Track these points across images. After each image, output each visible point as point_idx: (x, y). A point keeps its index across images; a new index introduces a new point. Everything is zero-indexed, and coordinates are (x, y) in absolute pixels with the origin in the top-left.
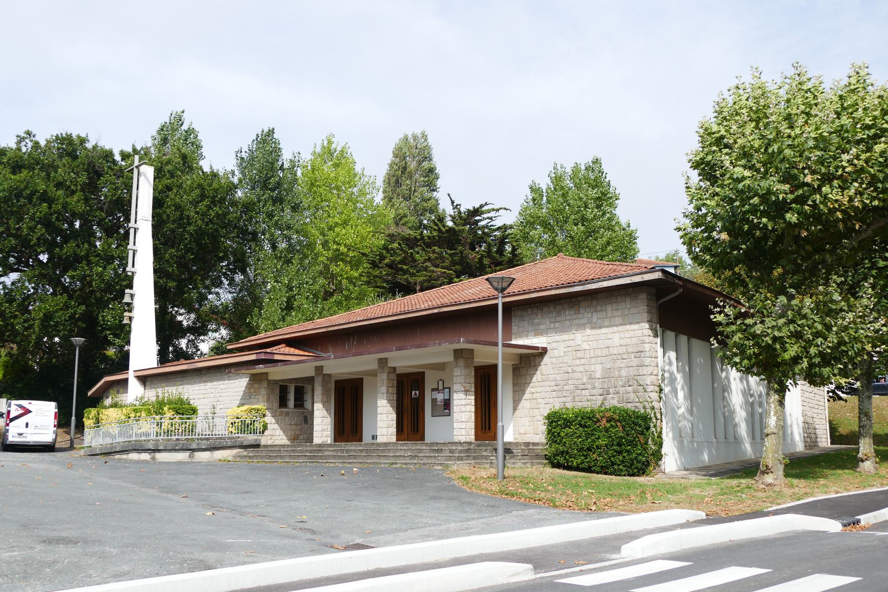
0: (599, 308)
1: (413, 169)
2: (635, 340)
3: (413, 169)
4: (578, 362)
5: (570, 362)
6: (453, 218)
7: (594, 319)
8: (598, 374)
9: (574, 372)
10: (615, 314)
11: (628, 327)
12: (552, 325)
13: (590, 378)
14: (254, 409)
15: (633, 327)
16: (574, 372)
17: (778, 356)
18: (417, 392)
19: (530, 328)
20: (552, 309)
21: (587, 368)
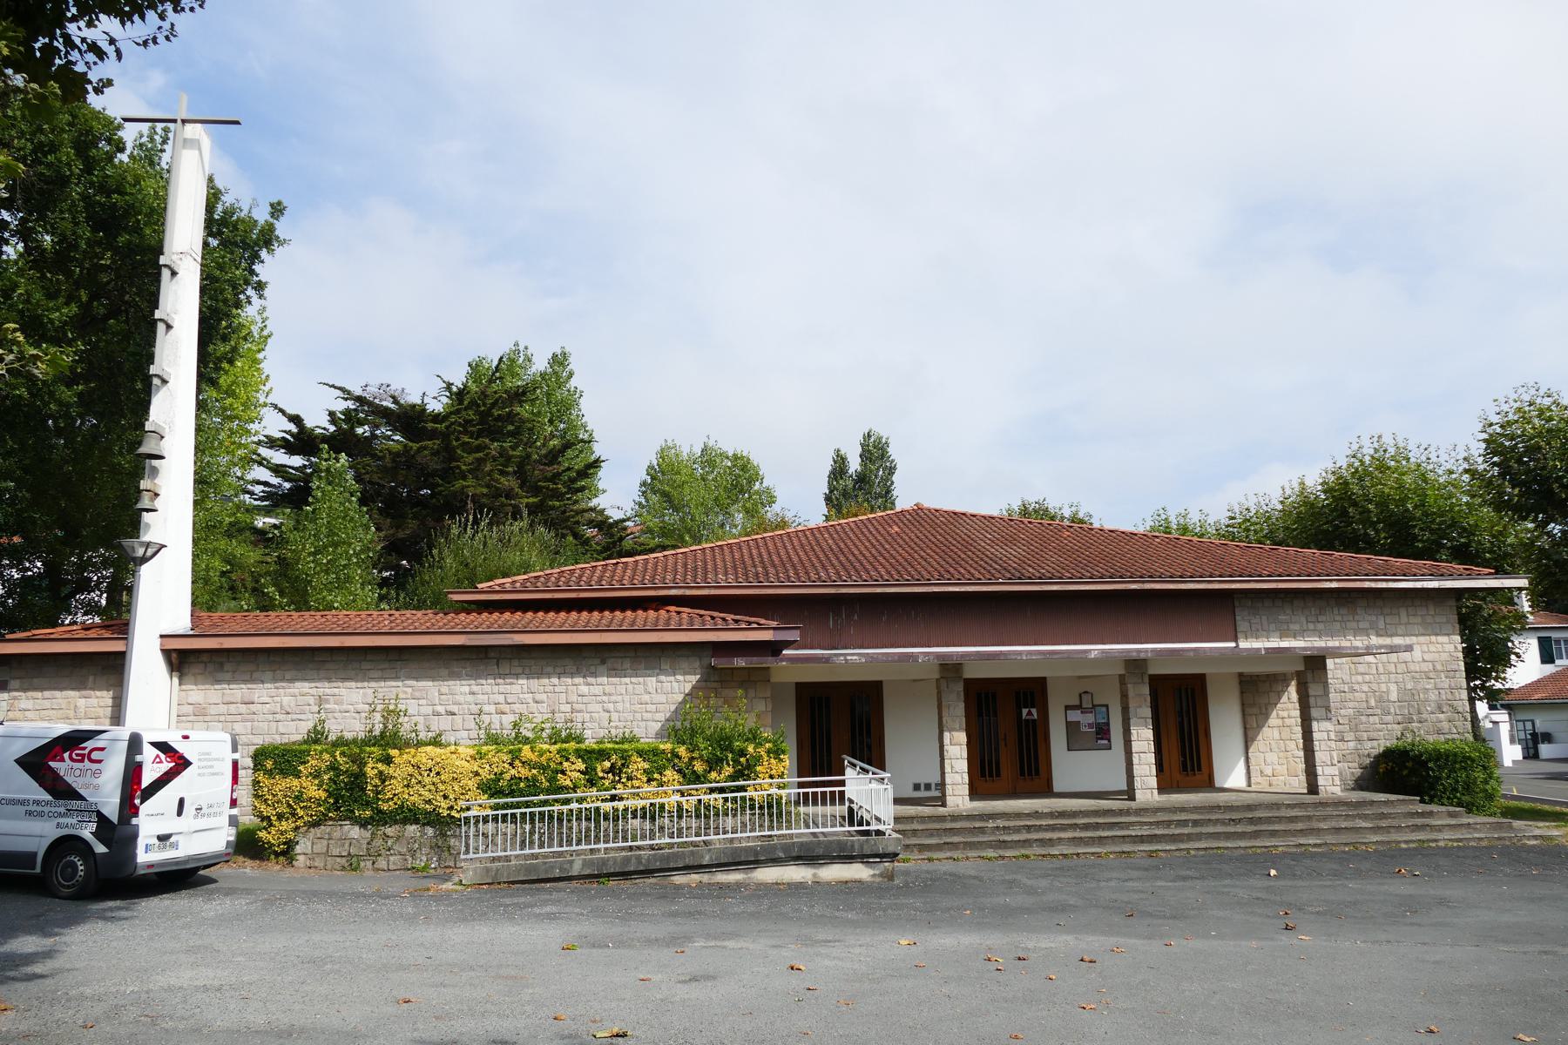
0: (1387, 610)
1: (861, 482)
2: (1445, 656)
3: (861, 482)
4: (1360, 678)
5: (1347, 678)
6: (1325, 492)
7: (1381, 624)
8: (1394, 696)
9: (1353, 690)
10: (1412, 619)
11: (1433, 638)
12: (1311, 626)
13: (1380, 700)
14: (506, 796)
15: (1442, 639)
16: (1353, 690)
17: (452, 517)
18: (1034, 711)
19: (1272, 626)
20: (1404, 619)
21: (1375, 686)
